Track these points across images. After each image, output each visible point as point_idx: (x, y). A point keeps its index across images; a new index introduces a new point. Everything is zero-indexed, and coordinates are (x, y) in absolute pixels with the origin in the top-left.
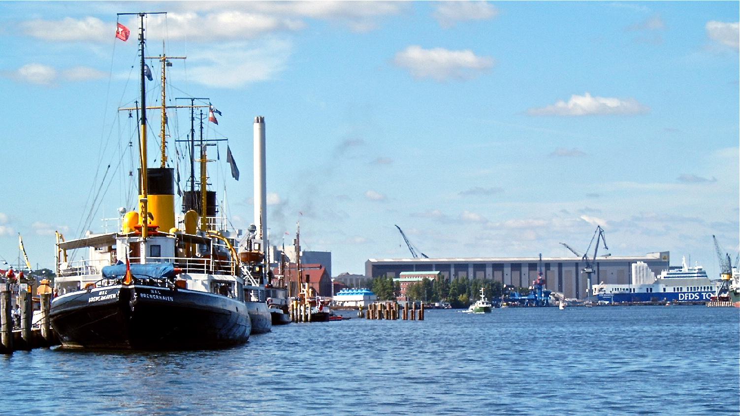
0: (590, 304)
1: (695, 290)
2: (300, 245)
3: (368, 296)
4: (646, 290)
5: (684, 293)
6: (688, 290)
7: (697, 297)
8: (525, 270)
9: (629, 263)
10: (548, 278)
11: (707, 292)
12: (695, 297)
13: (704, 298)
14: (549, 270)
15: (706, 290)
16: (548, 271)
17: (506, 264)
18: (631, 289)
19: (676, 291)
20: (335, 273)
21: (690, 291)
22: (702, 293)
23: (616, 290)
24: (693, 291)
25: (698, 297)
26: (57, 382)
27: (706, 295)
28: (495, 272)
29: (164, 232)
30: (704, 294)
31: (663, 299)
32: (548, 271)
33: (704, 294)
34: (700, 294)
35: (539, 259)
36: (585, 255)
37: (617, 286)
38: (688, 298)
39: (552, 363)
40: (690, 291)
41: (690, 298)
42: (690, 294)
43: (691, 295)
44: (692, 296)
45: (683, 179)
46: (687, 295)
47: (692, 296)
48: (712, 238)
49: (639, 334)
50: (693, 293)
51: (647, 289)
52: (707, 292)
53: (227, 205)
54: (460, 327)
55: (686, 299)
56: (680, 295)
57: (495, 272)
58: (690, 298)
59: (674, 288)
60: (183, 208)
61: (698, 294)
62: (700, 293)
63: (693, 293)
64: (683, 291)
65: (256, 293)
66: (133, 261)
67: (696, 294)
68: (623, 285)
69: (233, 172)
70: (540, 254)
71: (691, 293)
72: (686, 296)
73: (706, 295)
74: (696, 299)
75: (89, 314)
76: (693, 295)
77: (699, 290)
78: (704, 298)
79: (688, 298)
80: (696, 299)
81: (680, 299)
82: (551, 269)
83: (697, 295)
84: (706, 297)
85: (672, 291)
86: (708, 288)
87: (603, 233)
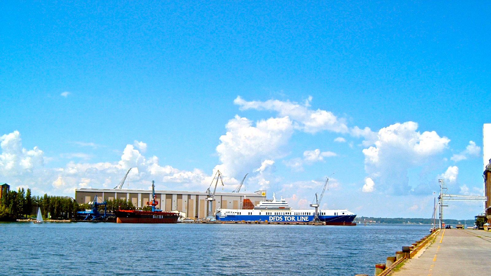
0: (158, 218)
1: (277, 214)
3: (209, 214)
5: (273, 216)
7: (281, 219)
8: (175, 197)
10: (165, 199)
11: (288, 216)
12: (280, 219)
13: (286, 220)
14: (190, 199)
15: (287, 215)
16: (189, 200)
18: (238, 213)
19: (268, 215)
20: (97, 197)
21: (276, 215)
24: (278, 215)
25: (282, 219)
28: (178, 199)
30: (286, 217)
31: (259, 219)
32: (189, 200)
37: (231, 210)
38: (275, 219)
40: (276, 215)
41: (276, 220)
42: (277, 217)
43: (271, 218)
44: (278, 218)
45: (348, 220)
50: (278, 216)
51: (249, 213)
52: (288, 216)
55: (274, 220)
56: (270, 217)
57: (178, 199)
59: (267, 213)
61: (282, 217)
63: (278, 216)
64: (272, 215)
67: (280, 217)
70: (153, 181)
71: (277, 216)
72: (274, 218)
73: (287, 218)
74: (280, 220)
75: (444, 222)
76: (278, 217)
77: (283, 215)
79: (275, 219)
80: (280, 220)
81: (270, 220)
82: (191, 198)
84: (291, 217)
85: (265, 214)
86: (288, 213)
87: (221, 175)
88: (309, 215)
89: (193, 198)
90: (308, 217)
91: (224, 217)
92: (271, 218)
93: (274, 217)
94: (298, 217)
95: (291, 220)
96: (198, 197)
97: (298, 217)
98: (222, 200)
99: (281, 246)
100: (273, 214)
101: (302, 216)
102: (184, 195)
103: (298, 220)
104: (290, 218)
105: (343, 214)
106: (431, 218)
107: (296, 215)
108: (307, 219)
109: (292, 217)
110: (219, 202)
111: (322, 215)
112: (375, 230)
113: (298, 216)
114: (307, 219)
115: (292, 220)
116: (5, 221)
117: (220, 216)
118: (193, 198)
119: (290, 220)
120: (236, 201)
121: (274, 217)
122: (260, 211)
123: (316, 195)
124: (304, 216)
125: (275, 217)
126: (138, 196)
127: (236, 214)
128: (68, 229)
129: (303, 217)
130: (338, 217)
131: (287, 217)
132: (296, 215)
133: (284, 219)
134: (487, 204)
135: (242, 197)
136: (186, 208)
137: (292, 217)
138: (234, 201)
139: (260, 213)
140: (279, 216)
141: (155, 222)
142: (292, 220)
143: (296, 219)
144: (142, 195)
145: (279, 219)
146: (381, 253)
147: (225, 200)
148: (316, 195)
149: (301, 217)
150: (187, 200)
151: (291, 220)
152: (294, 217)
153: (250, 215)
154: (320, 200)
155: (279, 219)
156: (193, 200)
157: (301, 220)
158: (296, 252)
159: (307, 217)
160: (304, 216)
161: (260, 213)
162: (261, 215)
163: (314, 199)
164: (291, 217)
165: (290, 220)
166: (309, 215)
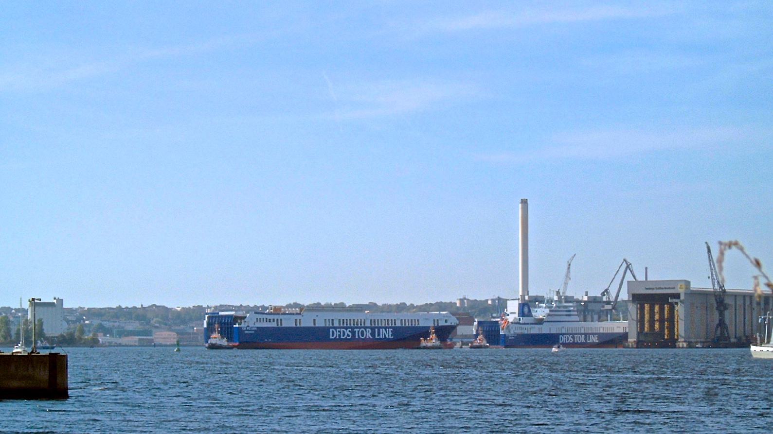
4: (433, 322)
5: (335, 328)
6: (340, 324)
9: (488, 300)
17: (739, 295)
22: (355, 330)
27: (358, 332)
36: (606, 290)
38: (340, 336)
39: (298, 402)
41: (342, 337)
42: (342, 330)
46: (339, 332)
49: (707, 378)
56: (331, 330)
60: (493, 300)
61: (350, 330)
62: (353, 328)
65: (596, 317)
68: (266, 326)
69: (161, 308)
71: (343, 328)
73: (358, 332)
78: (357, 337)
79: (340, 336)
81: (331, 337)
83: (349, 331)
84: (358, 336)
90: (392, 329)
91: (253, 332)
93: (338, 330)
94: (376, 330)
97: (376, 330)
99: (286, 418)
103: (377, 337)
106: (684, 322)
107: (373, 325)
109: (367, 330)
112: (463, 354)
116: (40, 398)
119: (363, 338)
124: (385, 328)
125: (339, 330)
128: (80, 422)
131: (359, 330)
132: (352, 325)
133: (353, 333)
134: (695, 294)
137: (367, 330)
139: (314, 320)
140: (346, 328)
141: (721, 346)
145: (346, 335)
146: (632, 393)
149: (381, 330)
151: (336, 336)
158: (426, 426)
160: (385, 328)
161: (314, 320)
165: (362, 336)
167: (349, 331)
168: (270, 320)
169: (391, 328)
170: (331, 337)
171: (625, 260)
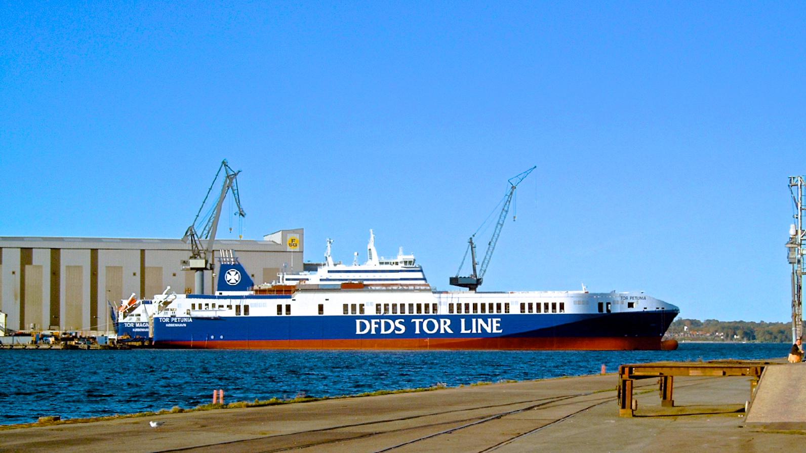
2: (338, 265)
5: (369, 318)
7: (400, 330)
11: (425, 318)
13: (417, 332)
14: (30, 263)
16: (27, 267)
19: (350, 314)
22: (413, 320)
23: (200, 305)
24: (390, 313)
25: (403, 328)
26: (17, 414)
27: (421, 324)
29: (292, 260)
32: (27, 267)
33: (417, 321)
34: (408, 322)
35: (50, 250)
38: (378, 330)
41: (383, 332)
42: (383, 321)
43: (363, 327)
44: (388, 326)
46: (376, 323)
47: (388, 326)
48: (534, 166)
52: (425, 318)
53: (796, 224)
54: (127, 372)
55: (373, 332)
56: (358, 322)
58: (383, 332)
66: (451, 308)
67: (397, 321)
72: (374, 326)
73: (421, 324)
74: (397, 332)
76: (390, 322)
78: (417, 332)
80: (397, 332)
81: (358, 332)
84: (370, 323)
85: (340, 313)
88: (503, 312)
89: (41, 259)
90: (499, 319)
91: (185, 325)
92: (363, 327)
93: (373, 321)
94: (463, 321)
95: (370, 330)
96: (144, 254)
97: (463, 321)
98: (147, 265)
100: (370, 311)
101: (479, 316)
102: (34, 248)
103: (463, 331)
104: (435, 321)
105: (631, 305)
108: (495, 325)
110: (134, 274)
111: (550, 312)
113: (463, 317)
114: (498, 328)
115: (442, 331)
117: (170, 322)
118: (41, 259)
120: (118, 267)
121: (373, 321)
122: (319, 298)
123: (471, 243)
126: (97, 252)
127: (232, 313)
129: (480, 321)
130: (648, 313)
133: (410, 326)
135: (215, 252)
136: (16, 296)
137: (442, 321)
138: (265, 270)
140: (394, 318)
142: (442, 331)
143: (455, 324)
144: (21, 251)
145: (392, 328)
147: (80, 265)
148: (471, 243)
149: (474, 320)
150: (19, 267)
151: (370, 330)
152: (449, 322)
153: (284, 314)
154: (486, 261)
155: (392, 328)
156: (40, 267)
157: (474, 331)
159: (495, 320)
162: (326, 313)
163: (467, 252)
164: (370, 323)
166: (503, 312)
167: (400, 323)
168: (207, 305)
169: (495, 316)
170: (358, 332)
171: (224, 163)
